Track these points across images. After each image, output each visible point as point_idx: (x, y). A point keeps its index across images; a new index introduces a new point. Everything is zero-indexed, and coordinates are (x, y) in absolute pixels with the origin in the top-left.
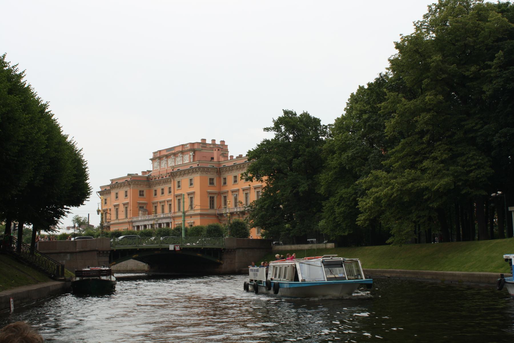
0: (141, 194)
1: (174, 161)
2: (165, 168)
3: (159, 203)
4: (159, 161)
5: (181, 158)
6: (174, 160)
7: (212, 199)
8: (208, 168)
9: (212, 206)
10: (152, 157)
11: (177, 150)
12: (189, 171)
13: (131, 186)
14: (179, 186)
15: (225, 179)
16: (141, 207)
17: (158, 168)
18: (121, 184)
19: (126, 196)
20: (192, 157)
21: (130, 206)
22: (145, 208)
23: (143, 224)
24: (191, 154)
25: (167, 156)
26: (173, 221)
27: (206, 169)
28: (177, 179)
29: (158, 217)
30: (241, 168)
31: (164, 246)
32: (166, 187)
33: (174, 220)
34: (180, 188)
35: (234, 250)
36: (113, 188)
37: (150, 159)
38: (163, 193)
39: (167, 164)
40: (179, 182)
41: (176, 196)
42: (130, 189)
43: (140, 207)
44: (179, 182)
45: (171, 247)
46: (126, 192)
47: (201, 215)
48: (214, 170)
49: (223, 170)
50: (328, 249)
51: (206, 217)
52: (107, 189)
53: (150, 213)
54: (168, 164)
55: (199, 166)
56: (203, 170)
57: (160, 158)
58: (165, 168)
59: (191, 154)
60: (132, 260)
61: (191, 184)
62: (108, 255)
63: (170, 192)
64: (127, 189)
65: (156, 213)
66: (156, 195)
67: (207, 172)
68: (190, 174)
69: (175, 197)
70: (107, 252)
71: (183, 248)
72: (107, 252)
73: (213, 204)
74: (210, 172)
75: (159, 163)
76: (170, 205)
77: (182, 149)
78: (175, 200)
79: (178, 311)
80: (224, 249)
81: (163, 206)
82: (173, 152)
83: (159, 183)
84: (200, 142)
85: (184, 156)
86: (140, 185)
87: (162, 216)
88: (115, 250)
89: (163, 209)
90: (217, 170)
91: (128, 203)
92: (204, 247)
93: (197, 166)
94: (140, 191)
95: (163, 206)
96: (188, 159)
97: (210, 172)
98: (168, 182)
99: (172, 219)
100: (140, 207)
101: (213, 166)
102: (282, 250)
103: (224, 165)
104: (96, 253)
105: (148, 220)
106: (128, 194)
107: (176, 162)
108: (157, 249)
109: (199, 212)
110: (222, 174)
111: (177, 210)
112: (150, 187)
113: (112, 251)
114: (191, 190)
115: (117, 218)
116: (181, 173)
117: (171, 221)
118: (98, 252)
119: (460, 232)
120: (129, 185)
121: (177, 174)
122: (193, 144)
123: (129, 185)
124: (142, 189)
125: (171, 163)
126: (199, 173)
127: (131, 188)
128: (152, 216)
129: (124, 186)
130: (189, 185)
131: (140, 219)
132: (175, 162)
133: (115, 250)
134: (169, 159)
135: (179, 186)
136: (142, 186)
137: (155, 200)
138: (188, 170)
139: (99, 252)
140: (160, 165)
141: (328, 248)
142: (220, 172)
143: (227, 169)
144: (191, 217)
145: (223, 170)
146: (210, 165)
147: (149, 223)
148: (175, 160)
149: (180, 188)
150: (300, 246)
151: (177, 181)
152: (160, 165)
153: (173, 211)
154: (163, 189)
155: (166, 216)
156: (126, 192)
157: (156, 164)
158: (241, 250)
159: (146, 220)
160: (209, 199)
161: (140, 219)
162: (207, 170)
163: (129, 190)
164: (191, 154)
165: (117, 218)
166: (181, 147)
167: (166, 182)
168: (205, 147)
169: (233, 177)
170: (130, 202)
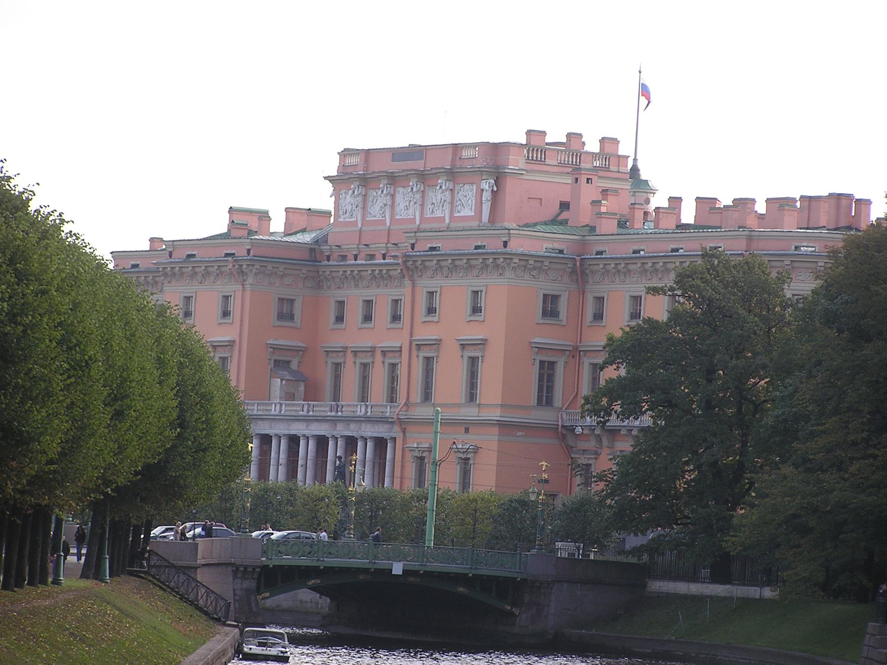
0: (285, 314)
1: (419, 202)
2: (383, 222)
3: (350, 355)
4: (362, 190)
5: (448, 193)
6: (418, 196)
7: (547, 371)
8: (539, 259)
9: (545, 397)
10: (334, 173)
11: (432, 163)
12: (473, 262)
13: (250, 280)
14: (431, 310)
15: (600, 300)
16: (281, 365)
17: (358, 215)
18: (456, 257)
19: (226, 314)
20: (487, 196)
21: (240, 351)
22: (294, 366)
23: (286, 432)
24: (485, 185)
25: (393, 179)
26: (401, 435)
27: (531, 262)
28: (426, 284)
29: (347, 412)
30: (657, 270)
31: (382, 564)
32: (383, 297)
33: (404, 431)
34: (436, 319)
35: (548, 584)
36: (174, 274)
37: (325, 178)
38: (368, 318)
39: (392, 206)
40: (431, 294)
41: (419, 346)
42: (244, 290)
43: (276, 362)
44: (431, 294)
45: (397, 569)
46: (226, 298)
47: (504, 426)
48: (563, 267)
49: (595, 268)
50: (766, 599)
51: (520, 433)
52: (142, 267)
53: (312, 394)
54: (397, 209)
55: (508, 250)
56: (524, 263)
57: (366, 181)
58: (383, 222)
59: (485, 185)
60: (305, 590)
61: (476, 310)
62: (256, 576)
63: (396, 318)
64: (232, 288)
65: (336, 397)
66: (340, 319)
67: (534, 273)
68: (475, 272)
69: (414, 347)
70: (254, 569)
71: (425, 571)
72: (254, 569)
73: (550, 389)
74: (546, 272)
75: (360, 199)
76: (393, 366)
77: (453, 160)
78: (414, 359)
79: (427, 249)
80: (524, 580)
81: (365, 366)
82: (419, 165)
83: (355, 278)
84: (523, 141)
85: (457, 187)
86: (283, 276)
87: (361, 411)
88: (271, 566)
89: (365, 379)
90: (575, 265)
91: (231, 344)
92: (474, 572)
93: (501, 250)
94: (281, 300)
95: (365, 366)
96: (472, 202)
97: (546, 272)
98: (390, 277)
99: (397, 428)
100: (276, 362)
101: (561, 252)
102: (667, 593)
103: (600, 249)
104: (230, 569)
105: (308, 420)
106: (235, 306)
107: (428, 207)
108: (366, 571)
109: (495, 415)
110: (591, 281)
111: (417, 396)
112: (319, 286)
113: (265, 568)
114: (475, 333)
115: (472, 397)
116: (443, 264)
117: (394, 435)
118: (235, 569)
119: (761, 600)
120: (242, 273)
121: (427, 264)
122: (496, 149)
123: (242, 273)
124: (287, 293)
125: (407, 208)
126: (508, 273)
127: (248, 287)
128: (323, 408)
129: (220, 274)
130: (469, 311)
131: (274, 410)
132: (422, 205)
133: (271, 566)
134: (401, 190)
135: (431, 310)
136: (288, 280)
137: (337, 341)
138: (470, 257)
139: (237, 568)
140: (364, 208)
141: (766, 597)
142: (583, 273)
143: (608, 267)
144: (467, 430)
145: (595, 268)
146: (550, 246)
147: (307, 433)
148: (423, 197)
149: (436, 319)
150: (707, 588)
151: (425, 290)
152: (364, 208)
153: (402, 398)
154: (368, 303)
155: (377, 412)
156: (226, 298)
157: (348, 199)
158: (565, 585)
159: (297, 419)
160: (535, 370)
161: (273, 412)
162: (538, 265)
163: (239, 295)
164: (487, 185)
165: (472, 397)
166: (450, 150)
167: (382, 277)
168: (542, 162)
169: (628, 298)
170: (241, 336)
